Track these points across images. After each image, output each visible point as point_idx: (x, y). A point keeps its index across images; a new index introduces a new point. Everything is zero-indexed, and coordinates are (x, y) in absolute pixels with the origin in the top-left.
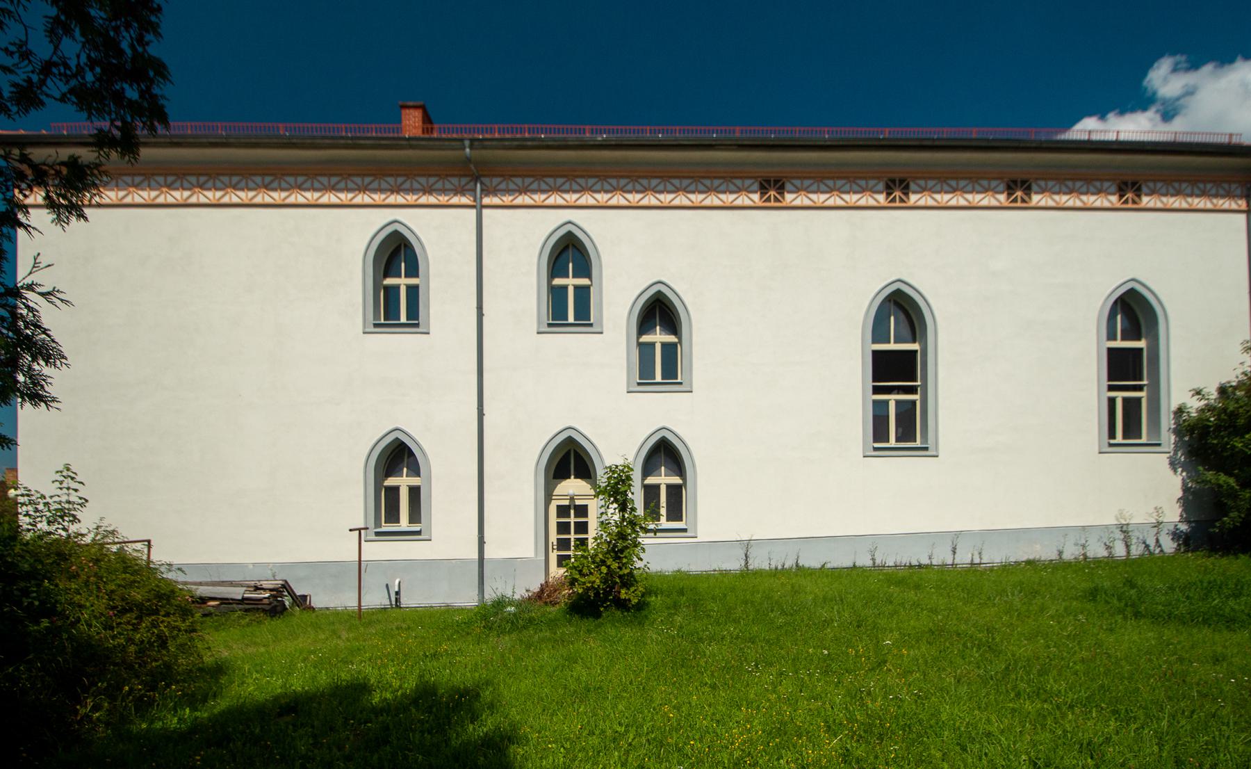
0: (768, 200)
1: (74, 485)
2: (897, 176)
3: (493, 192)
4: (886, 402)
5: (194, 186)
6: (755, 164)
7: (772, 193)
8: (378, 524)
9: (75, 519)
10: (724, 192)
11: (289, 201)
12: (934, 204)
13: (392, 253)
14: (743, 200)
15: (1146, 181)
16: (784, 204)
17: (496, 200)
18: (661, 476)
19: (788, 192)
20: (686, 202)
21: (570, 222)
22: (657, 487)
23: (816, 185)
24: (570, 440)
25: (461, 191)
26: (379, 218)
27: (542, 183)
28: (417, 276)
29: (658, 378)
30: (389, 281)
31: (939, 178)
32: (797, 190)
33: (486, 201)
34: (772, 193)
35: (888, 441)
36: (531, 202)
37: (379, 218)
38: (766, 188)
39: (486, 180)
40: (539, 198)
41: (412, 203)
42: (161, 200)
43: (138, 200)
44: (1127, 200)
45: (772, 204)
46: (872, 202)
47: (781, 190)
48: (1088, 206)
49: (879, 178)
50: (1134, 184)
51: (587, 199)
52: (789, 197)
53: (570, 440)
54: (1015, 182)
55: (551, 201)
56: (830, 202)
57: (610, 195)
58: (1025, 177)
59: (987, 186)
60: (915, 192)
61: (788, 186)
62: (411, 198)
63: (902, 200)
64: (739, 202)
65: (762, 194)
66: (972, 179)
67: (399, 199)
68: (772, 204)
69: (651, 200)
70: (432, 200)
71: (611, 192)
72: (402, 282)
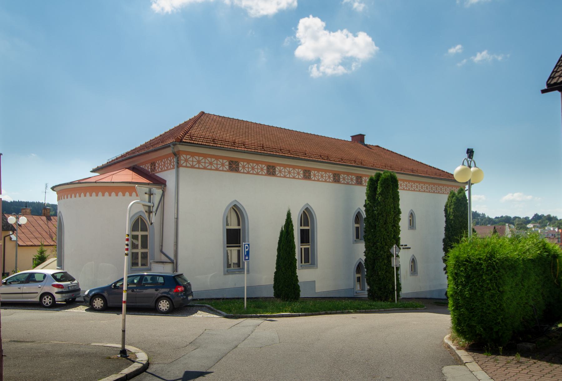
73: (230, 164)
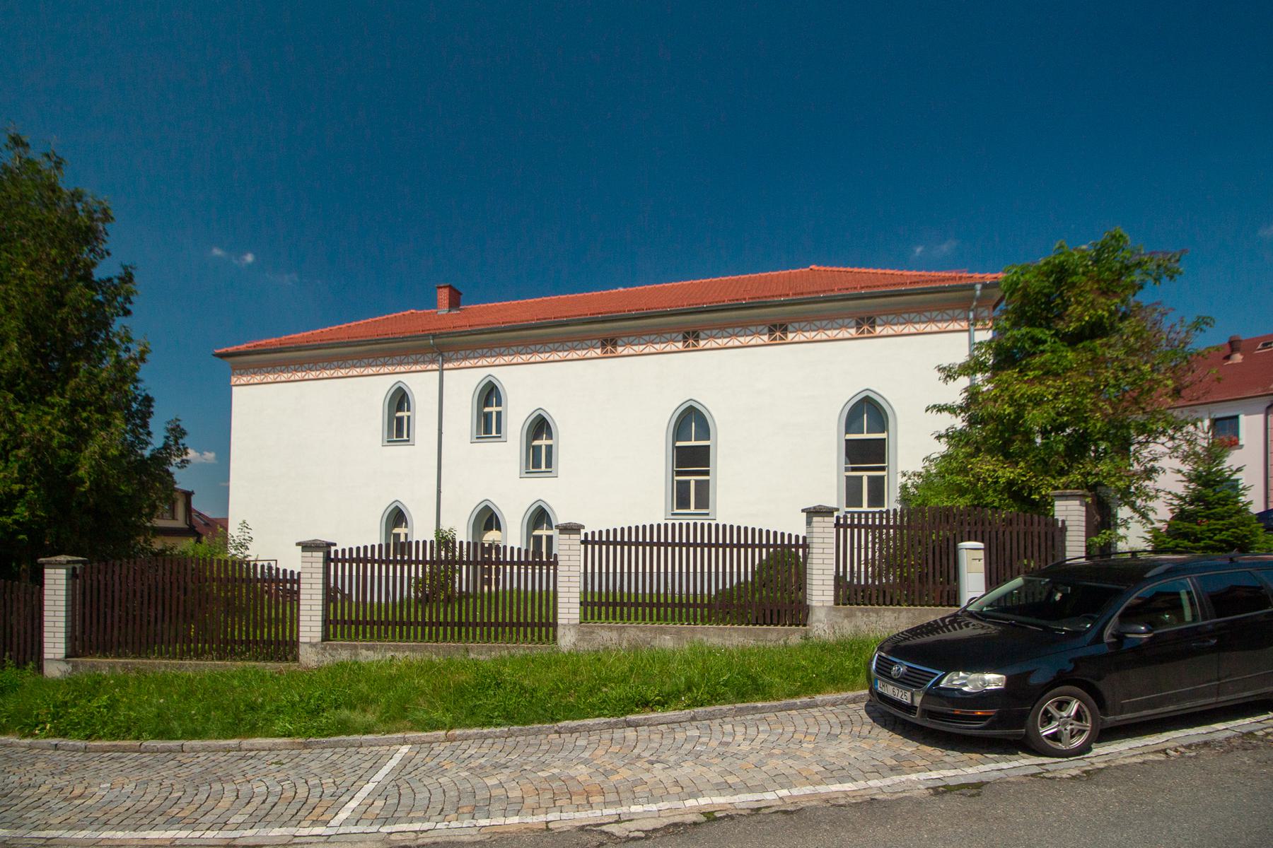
0: (606, 352)
1: (247, 530)
2: (690, 330)
3: (449, 360)
4: (688, 482)
5: (648, 343)
6: (597, 330)
7: (609, 348)
8: (673, 510)
9: (247, 548)
10: (896, 324)
11: (568, 357)
12: (717, 346)
13: (398, 404)
14: (591, 353)
15: (879, 316)
16: (616, 354)
17: (451, 365)
18: (883, 477)
19: (790, 332)
20: (803, 339)
21: (399, 382)
22: (541, 537)
23: (896, 319)
24: (487, 507)
25: (432, 361)
26: (392, 380)
27: (945, 315)
28: (501, 406)
30: (487, 410)
31: (720, 328)
32: (625, 345)
33: (446, 366)
34: (609, 348)
35: (689, 508)
36: (470, 365)
37: (392, 380)
38: (860, 324)
39: (446, 354)
40: (581, 353)
41: (392, 371)
42: (335, 375)
43: (325, 376)
44: (863, 331)
45: (609, 355)
46: (674, 348)
47: (615, 345)
48: (920, 331)
49: (679, 332)
50: (869, 318)
51: (500, 360)
52: (620, 349)
53: (487, 507)
54: (775, 326)
55: (480, 363)
56: (840, 336)
57: (512, 357)
58: (783, 322)
59: (819, 326)
60: (879, 325)
61: (620, 342)
62: (942, 326)
63: (869, 332)
64: (588, 355)
65: (858, 328)
66: (743, 327)
67: (402, 369)
68: (609, 355)
69: (650, 349)
70: (418, 368)
71: (905, 324)
72: (494, 409)
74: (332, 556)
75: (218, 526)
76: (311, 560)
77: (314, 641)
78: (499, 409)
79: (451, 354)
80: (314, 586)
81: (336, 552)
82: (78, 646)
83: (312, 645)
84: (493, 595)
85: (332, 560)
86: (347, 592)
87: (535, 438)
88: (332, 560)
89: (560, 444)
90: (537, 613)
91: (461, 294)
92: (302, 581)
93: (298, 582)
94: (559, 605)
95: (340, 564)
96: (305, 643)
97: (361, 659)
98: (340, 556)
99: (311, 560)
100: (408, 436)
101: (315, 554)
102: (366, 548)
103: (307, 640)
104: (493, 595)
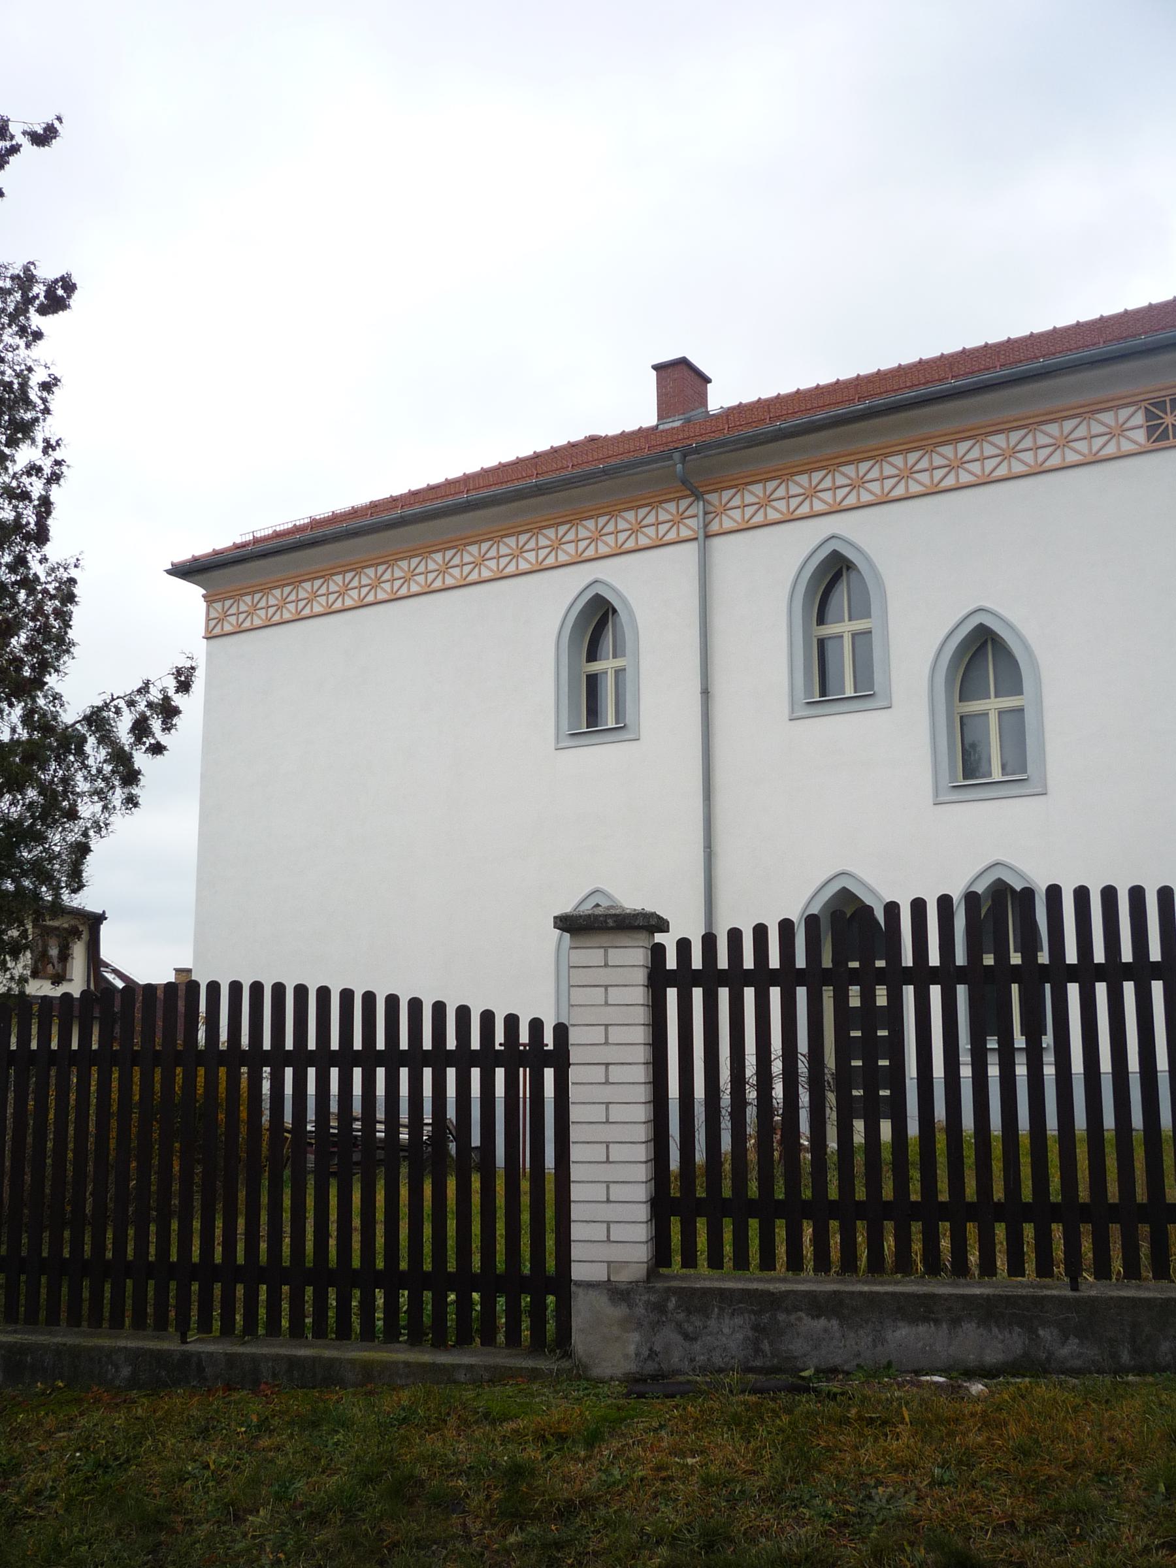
29: (997, 776)
39: (712, 497)
53: (845, 895)
73: (1149, 415)
74: (671, 963)
75: (150, 988)
76: (604, 976)
77: (624, 1277)
78: (859, 625)
79: (726, 495)
80: (616, 1074)
81: (684, 946)
82: (1023, 1276)
83: (617, 1292)
84: (832, 1159)
85: (671, 979)
86: (476, 1141)
87: (965, 695)
88: (671, 979)
89: (1049, 700)
90: (380, 1241)
91: (708, 381)
92: (575, 1055)
93: (560, 1059)
94: (576, 1212)
95: (697, 993)
96: (590, 1285)
97: (429, 1324)
98: (697, 963)
99: (604, 976)
100: (619, 714)
101: (616, 956)
102: (760, 932)
103: (598, 1273)
104: (832, 1159)
